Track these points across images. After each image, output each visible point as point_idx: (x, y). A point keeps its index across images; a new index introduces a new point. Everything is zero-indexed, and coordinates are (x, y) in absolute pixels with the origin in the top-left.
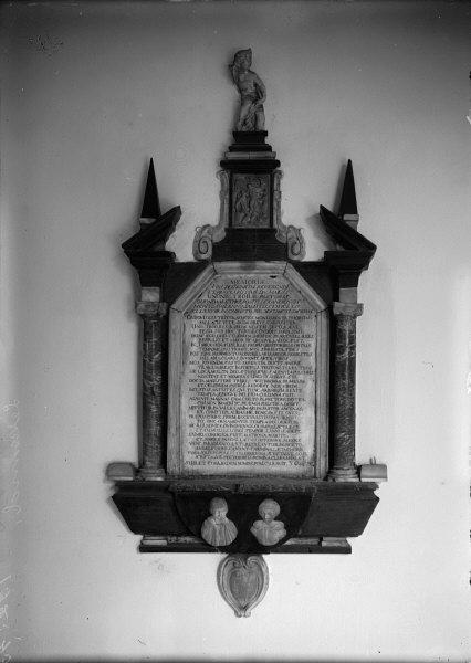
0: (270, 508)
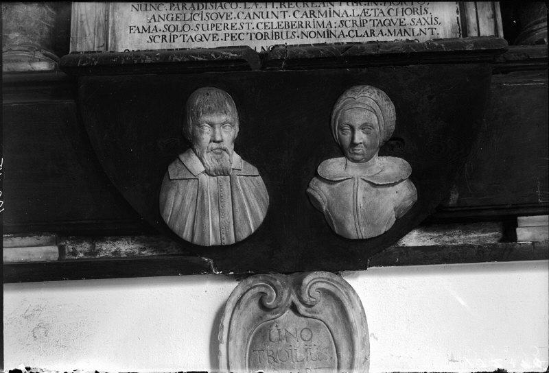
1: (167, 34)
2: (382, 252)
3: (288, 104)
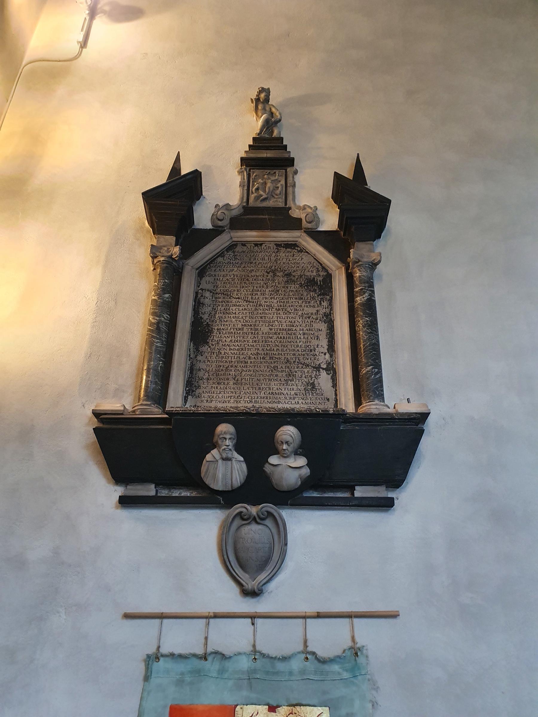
0: (288, 433)
1: (209, 399)
2: (294, 498)
3: (256, 434)
